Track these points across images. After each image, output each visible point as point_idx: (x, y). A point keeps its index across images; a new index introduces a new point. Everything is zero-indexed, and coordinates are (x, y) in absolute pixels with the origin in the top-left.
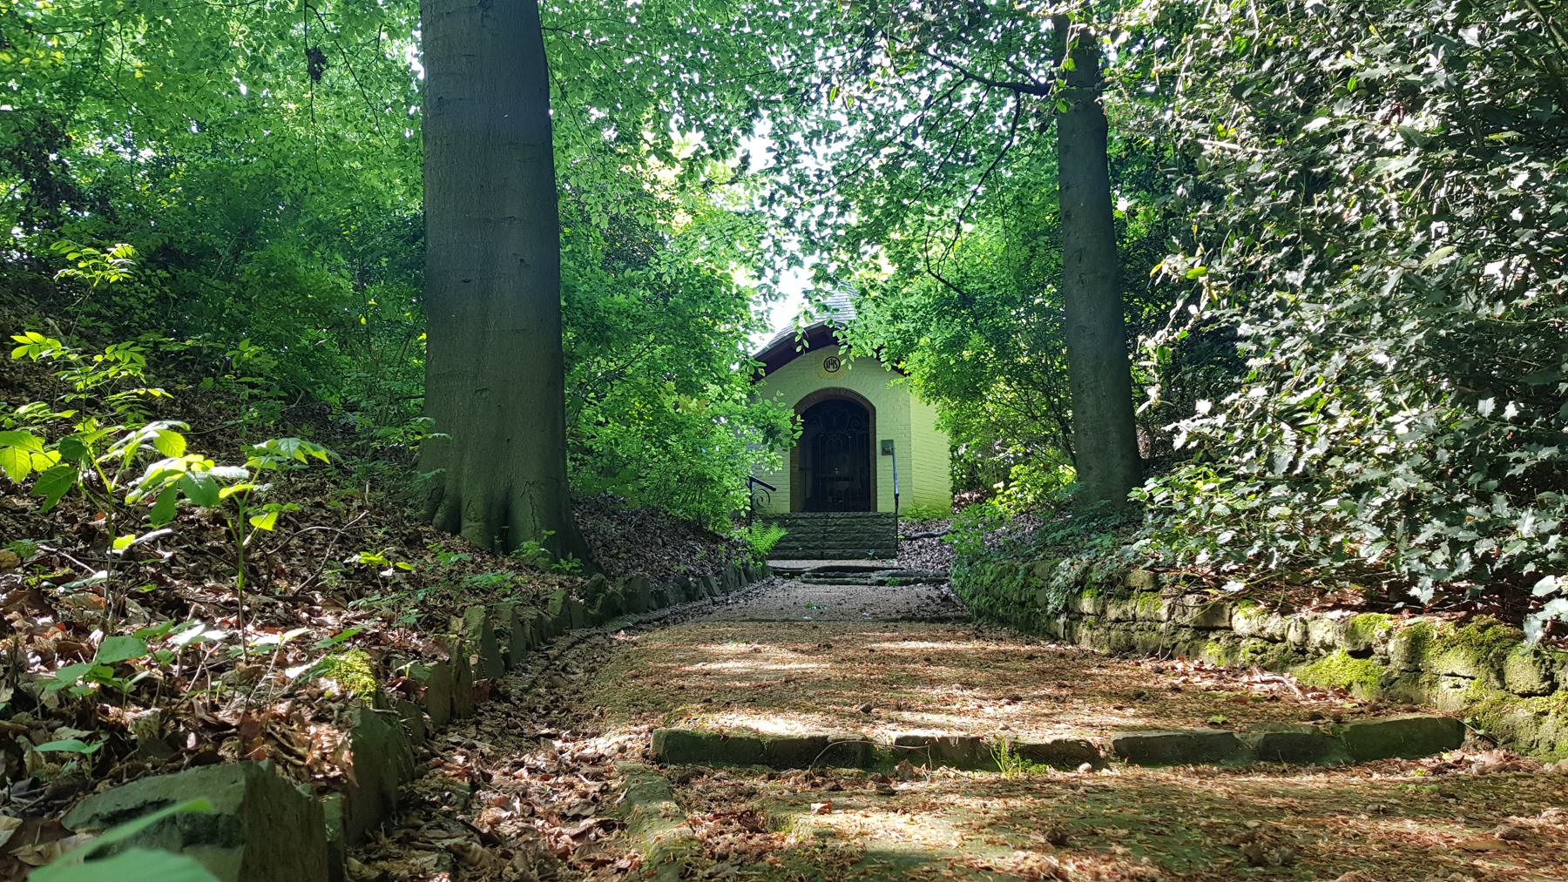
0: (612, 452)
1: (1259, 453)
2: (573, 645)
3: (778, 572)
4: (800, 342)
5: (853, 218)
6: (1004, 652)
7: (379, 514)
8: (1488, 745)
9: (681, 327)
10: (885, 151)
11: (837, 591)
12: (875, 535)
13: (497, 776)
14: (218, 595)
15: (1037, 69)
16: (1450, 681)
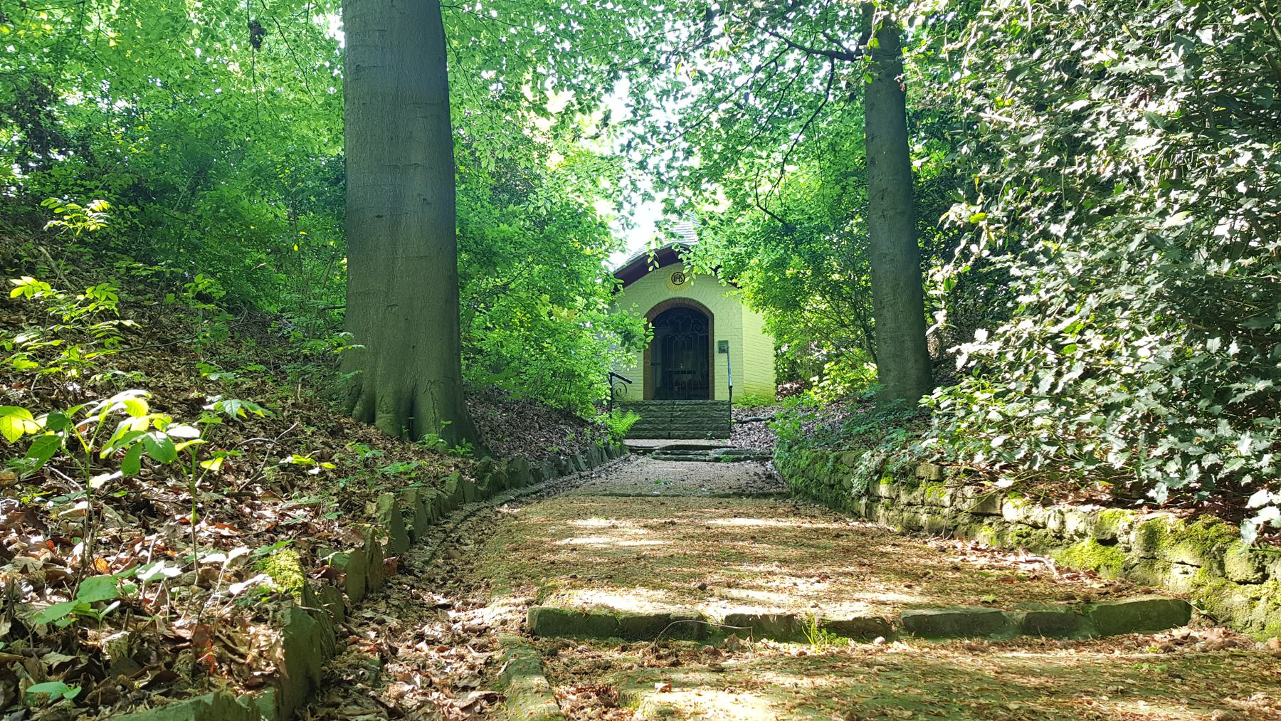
0: (498, 353)
1: (1026, 372)
2: (465, 518)
3: (633, 450)
4: (652, 263)
5: (696, 161)
6: (816, 530)
7: (309, 410)
8: (1210, 623)
9: (555, 251)
10: (723, 106)
11: (681, 467)
12: (712, 419)
13: (402, 651)
14: (177, 494)
15: (848, 39)
16: (1180, 568)
